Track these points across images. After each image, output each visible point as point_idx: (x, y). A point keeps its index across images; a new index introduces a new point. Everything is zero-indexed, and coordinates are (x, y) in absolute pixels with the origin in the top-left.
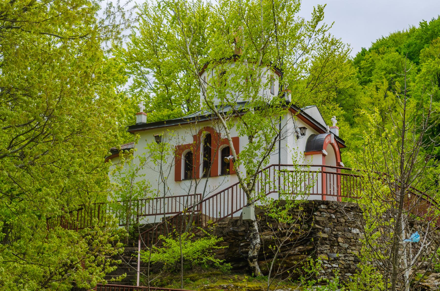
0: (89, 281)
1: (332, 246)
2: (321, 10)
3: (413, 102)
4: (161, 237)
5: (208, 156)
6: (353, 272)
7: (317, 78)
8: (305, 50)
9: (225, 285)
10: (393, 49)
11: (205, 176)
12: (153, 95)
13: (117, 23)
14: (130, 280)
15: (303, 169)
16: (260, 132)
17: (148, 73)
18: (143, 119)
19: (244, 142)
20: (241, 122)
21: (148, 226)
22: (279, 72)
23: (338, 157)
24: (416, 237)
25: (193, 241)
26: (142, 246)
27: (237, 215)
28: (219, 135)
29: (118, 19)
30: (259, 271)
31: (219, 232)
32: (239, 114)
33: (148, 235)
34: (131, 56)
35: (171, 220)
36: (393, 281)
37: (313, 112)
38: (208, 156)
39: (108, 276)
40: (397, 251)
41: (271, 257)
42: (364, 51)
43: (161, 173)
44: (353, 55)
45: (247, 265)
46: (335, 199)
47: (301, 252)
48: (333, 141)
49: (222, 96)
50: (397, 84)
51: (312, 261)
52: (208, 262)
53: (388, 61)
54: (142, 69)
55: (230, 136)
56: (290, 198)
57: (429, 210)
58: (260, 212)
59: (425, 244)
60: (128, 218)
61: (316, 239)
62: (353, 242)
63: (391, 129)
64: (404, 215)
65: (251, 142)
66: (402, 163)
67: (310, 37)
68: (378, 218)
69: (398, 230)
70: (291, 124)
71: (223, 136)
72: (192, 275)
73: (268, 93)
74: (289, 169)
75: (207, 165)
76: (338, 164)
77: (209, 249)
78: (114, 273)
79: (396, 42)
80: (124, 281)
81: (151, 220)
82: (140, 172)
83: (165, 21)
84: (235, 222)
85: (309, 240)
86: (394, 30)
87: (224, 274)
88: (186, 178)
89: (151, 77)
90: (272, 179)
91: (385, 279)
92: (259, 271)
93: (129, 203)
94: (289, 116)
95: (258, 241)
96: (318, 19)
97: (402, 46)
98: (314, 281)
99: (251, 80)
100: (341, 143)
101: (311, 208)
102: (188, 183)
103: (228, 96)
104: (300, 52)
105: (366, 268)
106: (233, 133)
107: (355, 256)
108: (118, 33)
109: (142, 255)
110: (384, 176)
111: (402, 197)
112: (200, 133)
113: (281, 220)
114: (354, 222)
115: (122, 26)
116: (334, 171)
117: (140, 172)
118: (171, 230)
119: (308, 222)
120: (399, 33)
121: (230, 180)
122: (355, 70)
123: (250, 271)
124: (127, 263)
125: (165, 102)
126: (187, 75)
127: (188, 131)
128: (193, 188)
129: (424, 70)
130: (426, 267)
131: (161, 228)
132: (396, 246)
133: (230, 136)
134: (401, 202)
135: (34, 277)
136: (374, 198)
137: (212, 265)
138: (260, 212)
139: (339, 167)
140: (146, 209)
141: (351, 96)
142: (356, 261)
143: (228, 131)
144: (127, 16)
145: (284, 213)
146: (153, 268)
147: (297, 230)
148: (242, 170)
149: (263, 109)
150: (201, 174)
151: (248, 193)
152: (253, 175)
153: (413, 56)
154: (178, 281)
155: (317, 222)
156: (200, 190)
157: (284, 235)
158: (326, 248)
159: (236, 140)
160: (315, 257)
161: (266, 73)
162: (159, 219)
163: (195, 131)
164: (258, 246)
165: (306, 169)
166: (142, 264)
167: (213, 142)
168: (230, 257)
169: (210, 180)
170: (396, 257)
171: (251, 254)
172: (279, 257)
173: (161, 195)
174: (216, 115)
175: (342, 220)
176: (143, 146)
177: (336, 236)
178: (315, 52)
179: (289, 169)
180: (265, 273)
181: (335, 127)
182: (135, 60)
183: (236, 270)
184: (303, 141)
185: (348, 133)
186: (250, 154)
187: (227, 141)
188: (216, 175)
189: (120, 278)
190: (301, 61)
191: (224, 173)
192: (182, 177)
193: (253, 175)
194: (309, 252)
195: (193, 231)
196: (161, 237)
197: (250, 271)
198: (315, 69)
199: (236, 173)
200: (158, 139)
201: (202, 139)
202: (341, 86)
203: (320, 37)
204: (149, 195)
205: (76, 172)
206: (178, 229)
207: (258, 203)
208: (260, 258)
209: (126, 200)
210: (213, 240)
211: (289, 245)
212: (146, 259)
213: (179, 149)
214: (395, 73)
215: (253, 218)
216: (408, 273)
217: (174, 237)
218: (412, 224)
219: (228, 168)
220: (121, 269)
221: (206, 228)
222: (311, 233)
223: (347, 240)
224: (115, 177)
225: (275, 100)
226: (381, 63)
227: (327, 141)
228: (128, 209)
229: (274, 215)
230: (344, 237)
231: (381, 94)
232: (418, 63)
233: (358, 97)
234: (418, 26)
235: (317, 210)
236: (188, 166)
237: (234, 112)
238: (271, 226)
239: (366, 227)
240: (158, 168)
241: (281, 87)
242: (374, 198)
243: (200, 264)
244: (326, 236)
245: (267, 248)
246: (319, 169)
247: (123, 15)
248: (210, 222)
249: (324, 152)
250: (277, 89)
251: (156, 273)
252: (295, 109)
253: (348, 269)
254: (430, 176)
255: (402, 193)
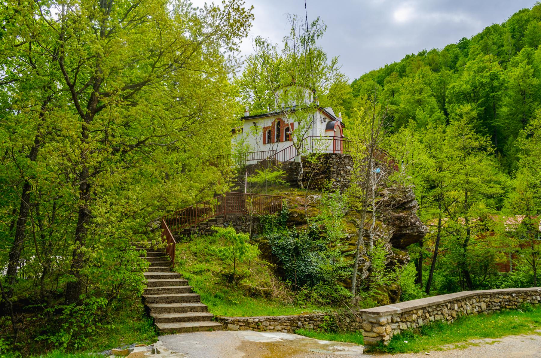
0: (222, 190)
1: (338, 175)
2: (336, 59)
3: (380, 105)
4: (257, 170)
5: (278, 132)
6: (347, 187)
7: (332, 95)
8: (327, 80)
9: (286, 193)
10: (371, 79)
11: (277, 142)
12: (252, 103)
13: (233, 65)
14: (242, 190)
15: (324, 138)
16: (304, 120)
17: (250, 92)
18: (248, 114)
19: (296, 125)
20: (295, 116)
21: (250, 165)
22: (314, 91)
23: (342, 133)
24: (378, 170)
25: (272, 172)
26: (248, 175)
27: (292, 160)
28: (284, 122)
29: (234, 63)
30: (302, 187)
31: (284, 168)
32: (293, 111)
33: (251, 170)
34: (242, 83)
35: (261, 162)
36: (367, 191)
37: (330, 110)
38: (278, 132)
39: (231, 188)
40: (369, 177)
41: (308, 179)
42: (356, 80)
43: (256, 140)
44: (350, 82)
45: (297, 184)
46: (339, 152)
47: (322, 177)
48: (339, 124)
49: (286, 102)
50: (372, 96)
51: (328, 182)
52: (279, 182)
53: (368, 85)
54: (248, 89)
55: (289, 123)
56: (318, 152)
57: (385, 158)
58: (303, 159)
59: (383, 174)
60: (241, 161)
61: (330, 171)
62: (347, 173)
63: (368, 119)
64: (373, 160)
65: (299, 125)
66: (372, 134)
67: (330, 73)
68: (360, 161)
69: (369, 167)
70: (319, 116)
71: (286, 122)
72: (271, 188)
73: (308, 101)
74: (318, 138)
75: (278, 136)
76: (341, 136)
77: (279, 176)
78: (234, 187)
79: (372, 75)
80: (238, 190)
81: (251, 163)
82: (247, 140)
83: (259, 66)
84: (291, 163)
85: (326, 172)
86: (371, 69)
87: (286, 188)
88: (268, 142)
89: (252, 94)
90: (309, 143)
91: (363, 190)
92: (302, 187)
93: (241, 155)
94: (318, 112)
95: (302, 172)
96: (334, 63)
97: (375, 77)
98: (328, 191)
99: (300, 95)
100: (343, 125)
101: (327, 157)
102: (269, 145)
103: (289, 103)
104: (325, 81)
105: (353, 185)
106: (291, 121)
107: (349, 179)
108: (234, 70)
109: (247, 179)
110: (364, 141)
111: (372, 151)
112: (275, 121)
113: (313, 162)
114: (348, 163)
115: (236, 66)
116: (340, 139)
117: (247, 140)
118: (261, 167)
119: (326, 163)
120: (374, 71)
121: (289, 143)
122: (351, 90)
123: (299, 187)
124: (240, 181)
125: (259, 105)
126: (269, 93)
127: (269, 120)
128: (271, 147)
129: (386, 89)
130: (383, 185)
131: (256, 166)
132: (368, 175)
133: (289, 123)
134: (371, 154)
135: (196, 188)
136: (358, 151)
137: (281, 183)
138: (303, 159)
139: (342, 137)
140: (250, 157)
141: (349, 103)
142: (349, 182)
143: (289, 120)
144: (238, 61)
145: (314, 158)
146: (252, 185)
147: (321, 167)
148: (295, 139)
149: (305, 109)
150: (275, 140)
151: (297, 150)
152: (300, 141)
153: (381, 82)
154: (265, 191)
155: (330, 163)
156: (275, 148)
157: (314, 169)
158: (335, 176)
159: (292, 124)
160: (329, 180)
161: (307, 92)
162: (255, 162)
163: (272, 120)
164: (302, 175)
165: (326, 138)
166: (248, 183)
167: (281, 125)
168: (288, 180)
169: (279, 143)
170: (368, 180)
171: (299, 178)
172: (312, 180)
173: (256, 150)
174: (283, 112)
175: (343, 162)
176: (248, 127)
177: (340, 170)
178: (332, 81)
179: (318, 138)
180: (305, 187)
181: (340, 117)
182: (244, 85)
183: (292, 186)
184: (325, 124)
185: (347, 120)
186: (299, 131)
187: (288, 124)
188: (283, 141)
189: (236, 189)
190: (325, 85)
191: (286, 140)
192: (267, 142)
193: (300, 141)
194: (326, 178)
195: (272, 167)
196: (257, 170)
197: (299, 187)
198: (332, 89)
199: (292, 140)
200: (255, 124)
201: (276, 124)
202: (345, 97)
203: (335, 73)
204: (250, 151)
205: (215, 138)
206: (264, 167)
207: (303, 155)
208: (303, 180)
209: (240, 153)
210: (281, 172)
211: (316, 174)
212: (249, 180)
213: (265, 129)
214: (371, 91)
215: (300, 161)
216: (374, 188)
217: (263, 170)
218: (376, 164)
219: (288, 138)
220: (237, 184)
221: (278, 166)
222: (328, 169)
223: (345, 172)
224: (234, 142)
225: (311, 104)
226: (365, 86)
227: (336, 124)
228: (241, 157)
229: (310, 160)
230: (343, 170)
231: (364, 102)
232: (383, 86)
233: (353, 103)
234: (384, 67)
235: (331, 157)
236: (269, 137)
237: (291, 110)
238: (308, 165)
239: (354, 166)
240: (255, 138)
241: (314, 98)
242: (358, 151)
243: (275, 183)
244: (334, 170)
245: (306, 176)
246: (332, 138)
247: (236, 60)
248: (280, 163)
249: (335, 130)
250: (312, 99)
251: (254, 187)
252: (321, 109)
253: (345, 186)
254: (387, 142)
255: (372, 149)
